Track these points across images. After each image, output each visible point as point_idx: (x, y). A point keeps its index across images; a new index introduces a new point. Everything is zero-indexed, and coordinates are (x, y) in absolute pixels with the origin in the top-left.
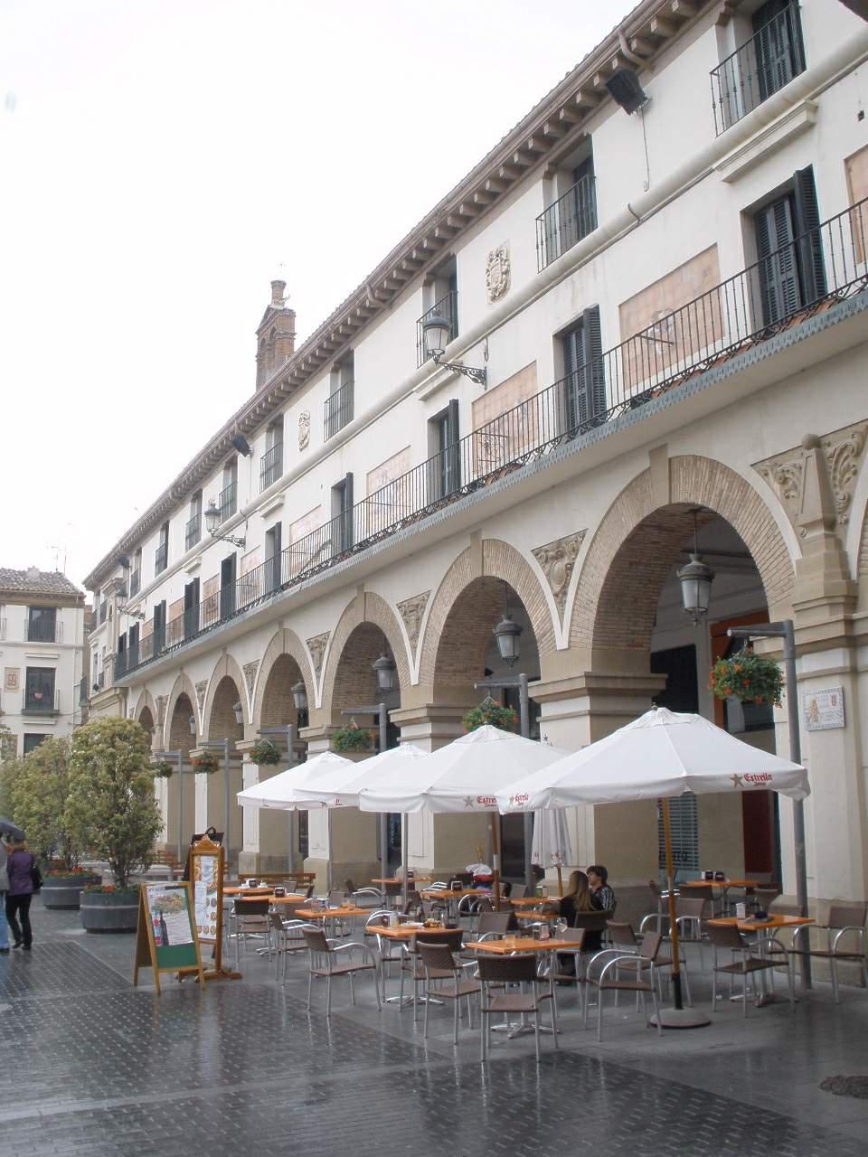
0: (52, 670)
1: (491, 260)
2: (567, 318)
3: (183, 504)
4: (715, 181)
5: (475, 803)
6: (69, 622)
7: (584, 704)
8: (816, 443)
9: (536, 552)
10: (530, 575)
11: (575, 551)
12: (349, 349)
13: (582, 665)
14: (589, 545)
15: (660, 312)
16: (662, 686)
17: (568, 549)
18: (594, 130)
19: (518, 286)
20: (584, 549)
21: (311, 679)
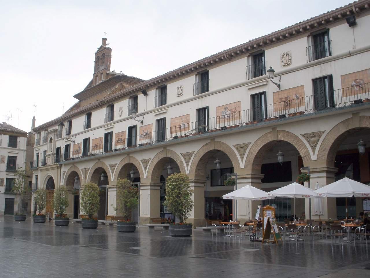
0: (16, 157)
1: (284, 55)
2: (200, 107)
3: (230, 61)
4: (103, 129)
5: (364, 195)
6: (22, 142)
7: (324, 174)
8: (85, 169)
9: (141, 161)
10: (140, 165)
11: (115, 166)
12: (91, 112)
13: (149, 181)
14: (326, 134)
15: (357, 79)
16: (263, 177)
17: (114, 166)
18: (266, 50)
19: (122, 117)
20: (150, 162)
21: (183, 164)
